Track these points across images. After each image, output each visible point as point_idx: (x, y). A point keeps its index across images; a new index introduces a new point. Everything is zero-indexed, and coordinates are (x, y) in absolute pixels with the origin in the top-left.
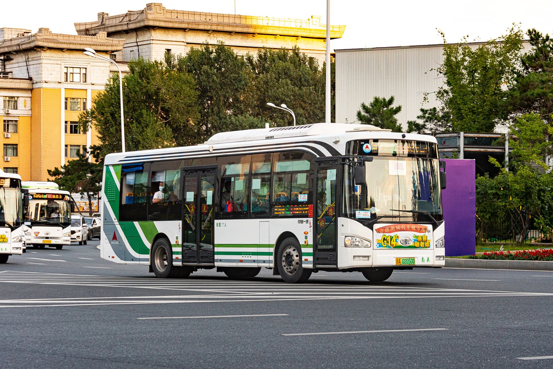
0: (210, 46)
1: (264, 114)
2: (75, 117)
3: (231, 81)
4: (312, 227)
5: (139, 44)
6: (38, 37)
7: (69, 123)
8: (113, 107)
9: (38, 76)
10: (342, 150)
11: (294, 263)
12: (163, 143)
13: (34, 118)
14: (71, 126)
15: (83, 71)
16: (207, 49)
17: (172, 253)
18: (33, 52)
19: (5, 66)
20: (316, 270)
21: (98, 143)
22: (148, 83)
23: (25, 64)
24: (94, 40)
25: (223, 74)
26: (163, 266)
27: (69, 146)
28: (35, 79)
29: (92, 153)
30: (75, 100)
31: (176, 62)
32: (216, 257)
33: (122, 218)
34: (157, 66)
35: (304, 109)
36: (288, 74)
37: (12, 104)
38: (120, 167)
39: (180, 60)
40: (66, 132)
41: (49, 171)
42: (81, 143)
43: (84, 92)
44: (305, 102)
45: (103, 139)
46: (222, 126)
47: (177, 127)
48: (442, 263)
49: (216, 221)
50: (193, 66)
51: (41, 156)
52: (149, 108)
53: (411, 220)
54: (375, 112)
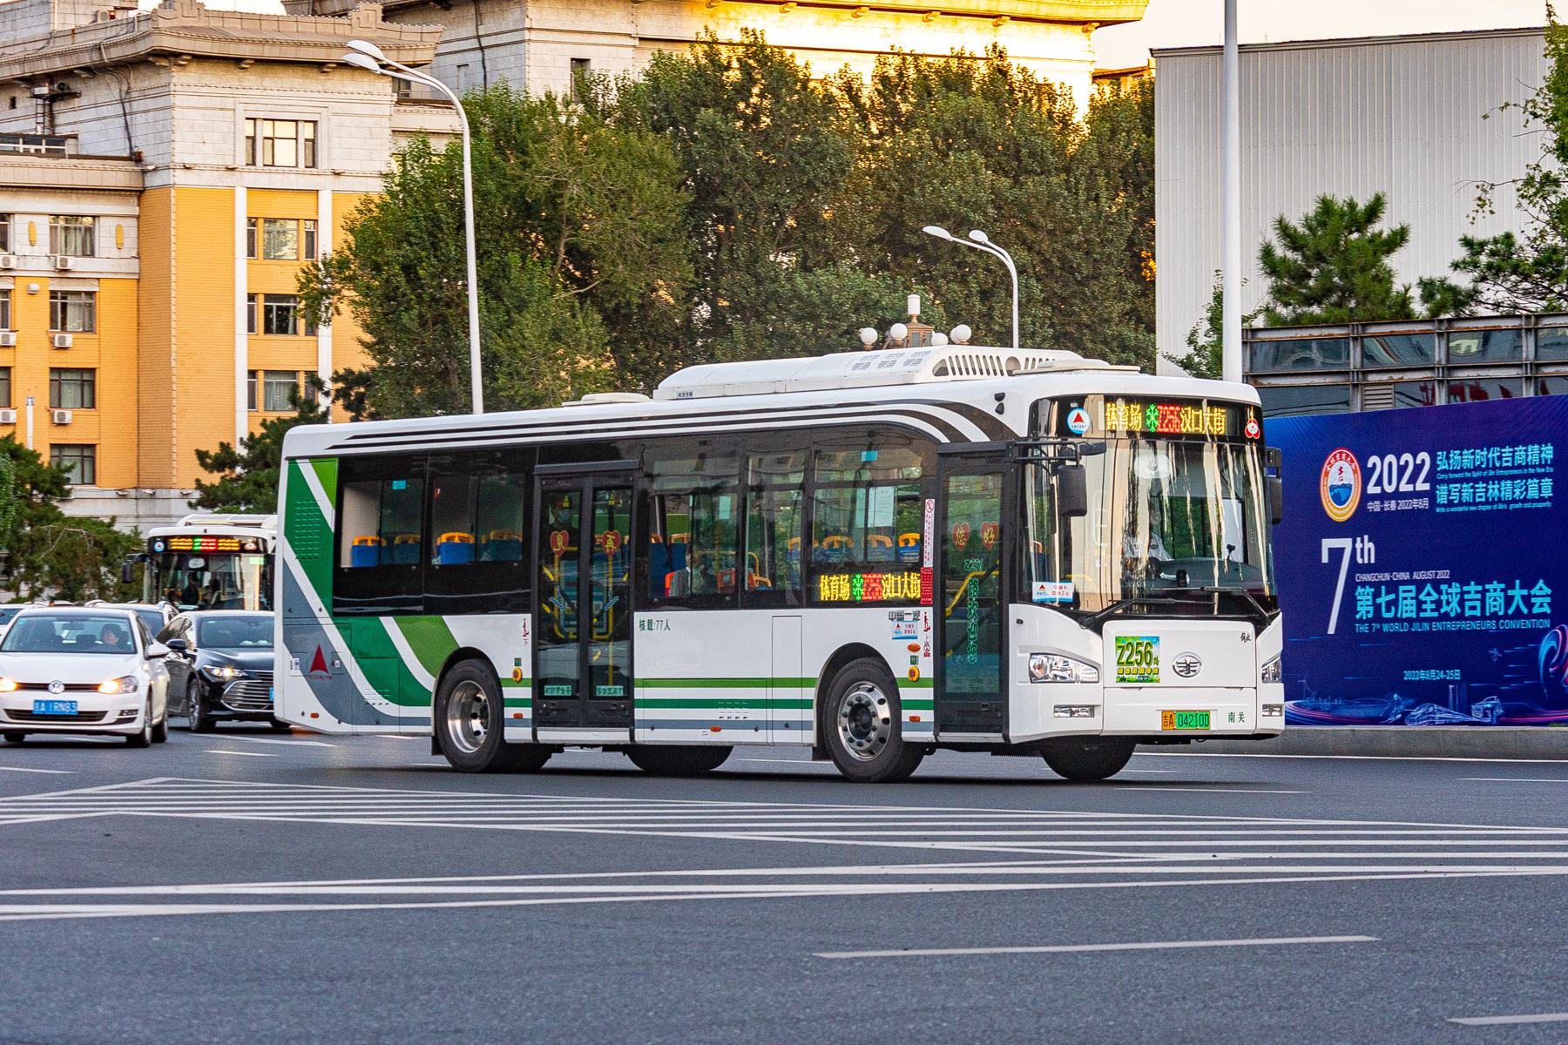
0: (723, 49)
1: (900, 266)
2: (285, 281)
3: (791, 159)
4: (529, 637)
5: (485, 42)
6: (162, 24)
7: (261, 299)
8: (411, 244)
9: (162, 148)
11: (875, 723)
12: (574, 362)
13: (149, 284)
14: (268, 310)
15: (307, 131)
16: (712, 56)
17: (502, 703)
18: (143, 69)
19: (52, 116)
21: (363, 362)
22: (525, 165)
23: (118, 109)
24: (340, 30)
25: (765, 138)
26: (472, 735)
27: (261, 375)
28: (151, 159)
29: (339, 394)
30: (278, 225)
31: (613, 99)
34: (555, 113)
35: (1030, 249)
36: (978, 135)
37: (76, 239)
38: (336, 464)
39: (629, 94)
40: (251, 328)
41: (202, 456)
42: (301, 364)
43: (311, 198)
44: (1033, 226)
45: (374, 348)
46: (765, 304)
47: (617, 309)
48: (1277, 723)
49: (638, 616)
50: (666, 109)
51: (169, 407)
52: (525, 247)
54: (1324, 245)
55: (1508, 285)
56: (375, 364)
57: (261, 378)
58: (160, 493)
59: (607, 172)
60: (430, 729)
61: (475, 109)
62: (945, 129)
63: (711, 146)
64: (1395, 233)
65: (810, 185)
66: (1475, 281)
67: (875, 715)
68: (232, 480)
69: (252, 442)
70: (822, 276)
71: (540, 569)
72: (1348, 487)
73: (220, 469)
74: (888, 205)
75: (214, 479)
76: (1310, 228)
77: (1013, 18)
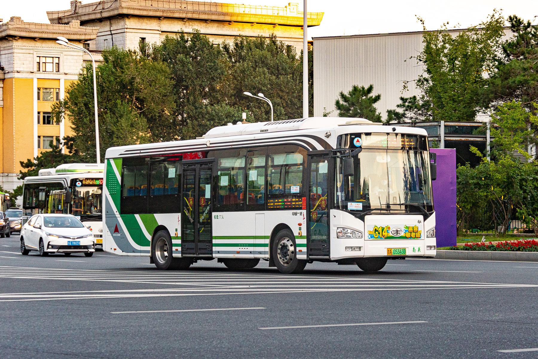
0: (185, 35)
1: (240, 103)
2: (48, 107)
3: (206, 70)
4: (180, 222)
5: (113, 32)
6: (10, 27)
8: (87, 97)
10: (333, 143)
11: (289, 253)
14: (44, 117)
15: (56, 60)
16: (182, 38)
17: (171, 245)
20: (311, 261)
22: (122, 72)
24: (67, 29)
25: (198, 63)
26: (163, 257)
27: (42, 137)
28: (7, 69)
29: (65, 144)
30: (48, 90)
31: (151, 51)
32: (215, 249)
33: (122, 212)
35: (281, 98)
38: (121, 161)
40: (39, 123)
41: (22, 163)
42: (55, 134)
44: (282, 91)
45: (76, 130)
47: (152, 117)
48: (433, 252)
49: (214, 214)
51: (13, 147)
52: (123, 98)
53: (404, 212)
54: (354, 100)
55: (414, 112)
56: (76, 134)
60: (150, 254)
61: (106, 55)
62: (255, 61)
64: (376, 97)
65: (212, 78)
66: (404, 111)
67: (289, 250)
69: (38, 159)
70: (217, 107)
71: (183, 198)
73: (28, 167)
74: (237, 85)
75: (25, 170)
76: (350, 95)
77: (279, 25)
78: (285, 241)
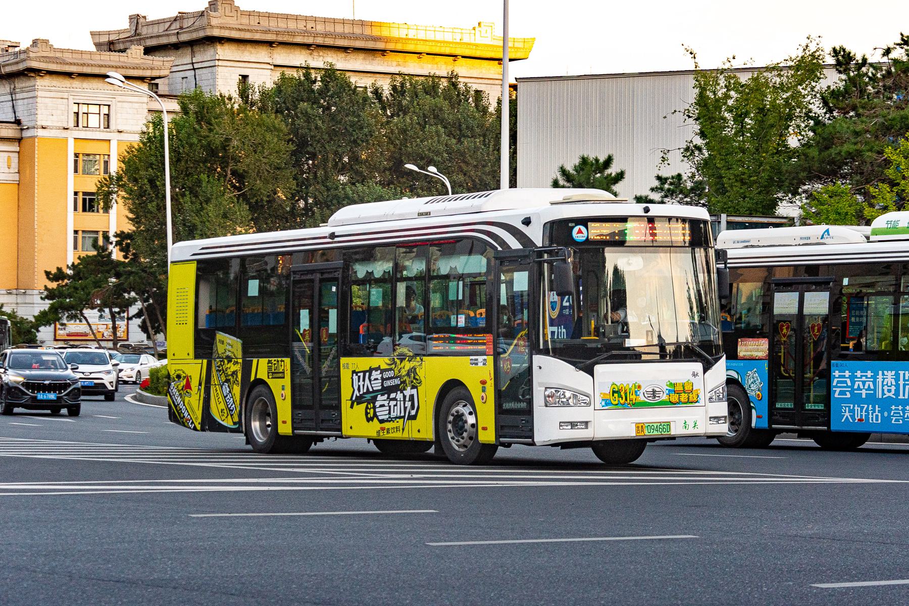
0: (312, 71)
1: (399, 182)
3: (346, 128)
5: (196, 66)
6: (31, 55)
9: (32, 117)
14: (84, 200)
15: (105, 110)
16: (307, 76)
21: (129, 228)
22: (210, 130)
25: (333, 117)
26: (264, 428)
27: (80, 233)
28: (25, 122)
29: (118, 243)
31: (257, 97)
35: (465, 174)
38: (238, 260)
39: (264, 94)
40: (75, 209)
41: (48, 274)
42: (101, 228)
43: (106, 144)
47: (257, 202)
48: (723, 428)
51: (34, 248)
53: (658, 357)
56: (134, 228)
57: (80, 234)
58: (28, 292)
59: (252, 134)
63: (305, 122)
67: (466, 422)
68: (63, 286)
72: (556, 302)
73: (57, 280)
74: (394, 152)
75: (53, 285)
77: (463, 57)
78: (460, 408)
